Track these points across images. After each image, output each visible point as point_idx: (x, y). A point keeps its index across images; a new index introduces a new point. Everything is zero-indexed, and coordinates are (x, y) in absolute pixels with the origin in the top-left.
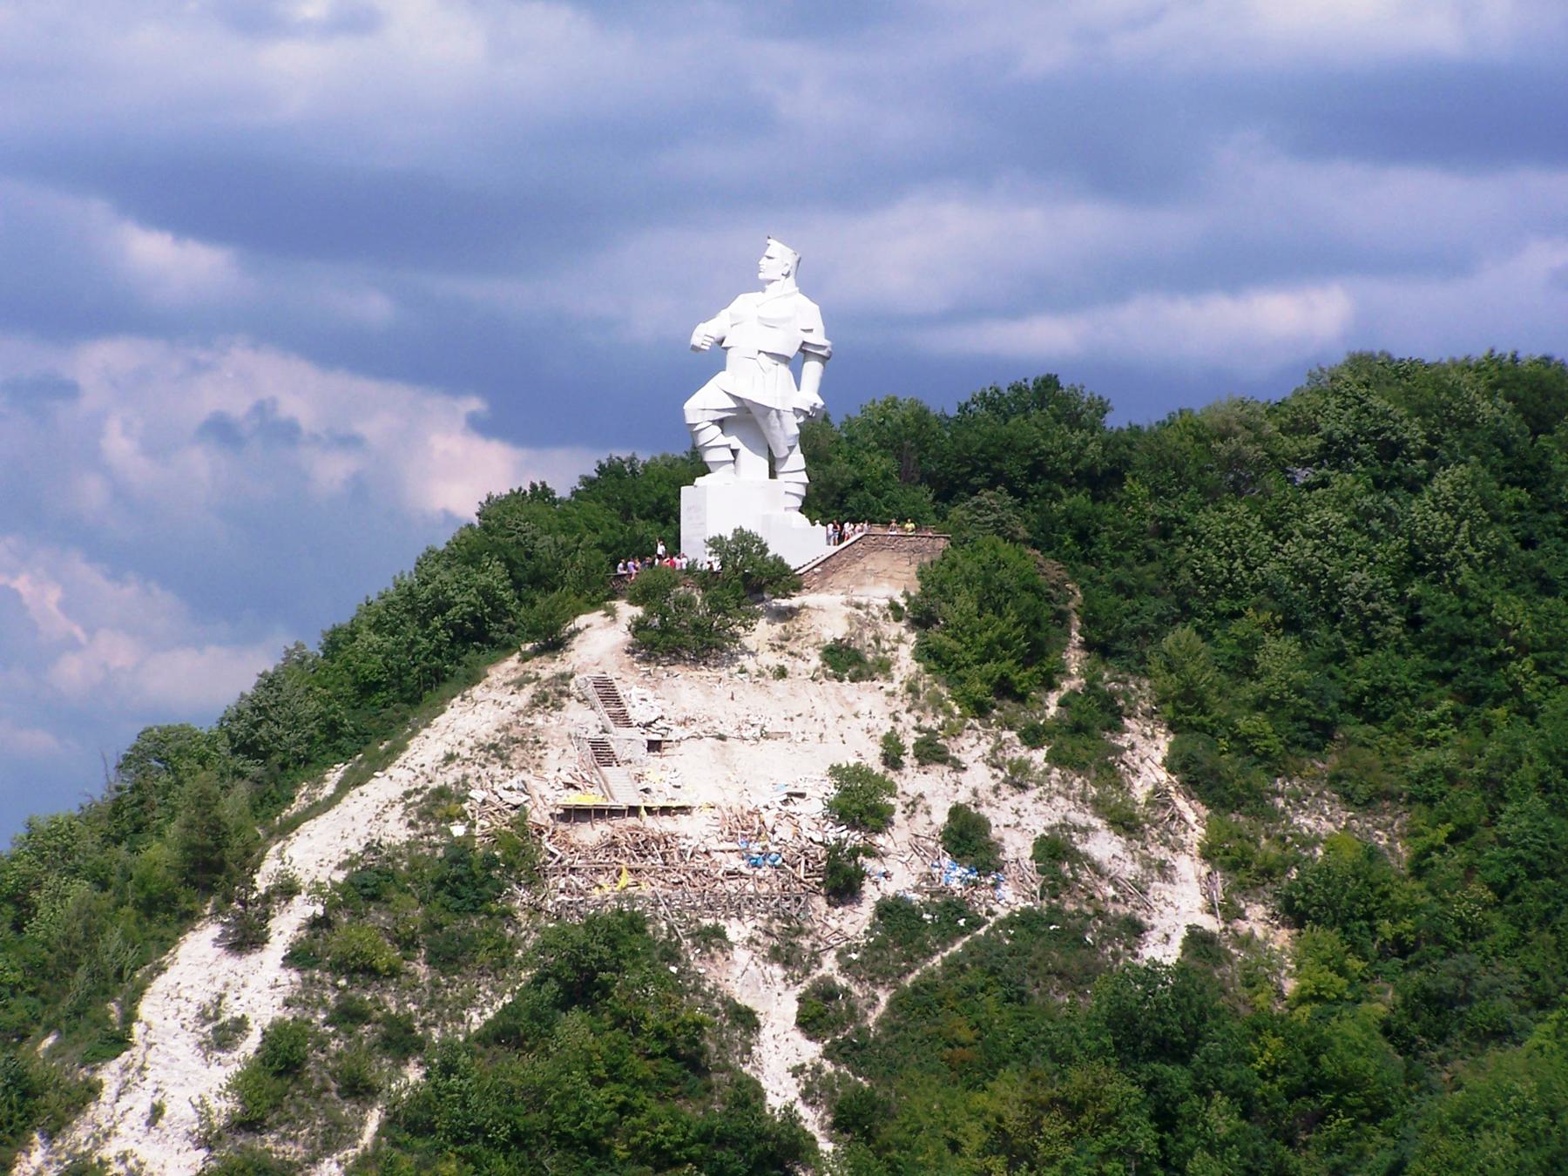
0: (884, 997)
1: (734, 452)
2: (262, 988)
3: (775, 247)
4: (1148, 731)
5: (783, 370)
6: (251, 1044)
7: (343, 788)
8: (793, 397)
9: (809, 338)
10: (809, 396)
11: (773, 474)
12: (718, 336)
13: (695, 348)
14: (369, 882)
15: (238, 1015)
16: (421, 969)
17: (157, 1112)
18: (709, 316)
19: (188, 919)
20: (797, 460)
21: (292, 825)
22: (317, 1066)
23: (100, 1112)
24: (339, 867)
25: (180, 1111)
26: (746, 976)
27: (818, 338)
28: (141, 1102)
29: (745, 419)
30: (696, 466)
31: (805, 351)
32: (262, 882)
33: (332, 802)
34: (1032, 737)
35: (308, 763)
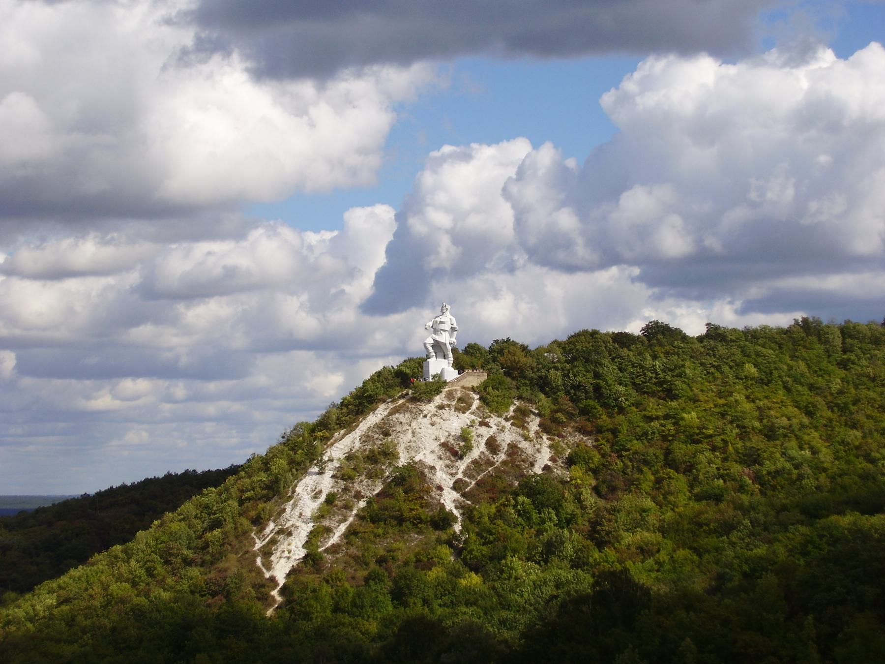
0: (473, 482)
2: (327, 483)
4: (380, 531)
6: (323, 498)
20: (451, 355)
21: (332, 444)
23: (286, 515)
26: (442, 477)
27: (455, 326)
28: (297, 512)
32: (325, 458)
34: (507, 419)
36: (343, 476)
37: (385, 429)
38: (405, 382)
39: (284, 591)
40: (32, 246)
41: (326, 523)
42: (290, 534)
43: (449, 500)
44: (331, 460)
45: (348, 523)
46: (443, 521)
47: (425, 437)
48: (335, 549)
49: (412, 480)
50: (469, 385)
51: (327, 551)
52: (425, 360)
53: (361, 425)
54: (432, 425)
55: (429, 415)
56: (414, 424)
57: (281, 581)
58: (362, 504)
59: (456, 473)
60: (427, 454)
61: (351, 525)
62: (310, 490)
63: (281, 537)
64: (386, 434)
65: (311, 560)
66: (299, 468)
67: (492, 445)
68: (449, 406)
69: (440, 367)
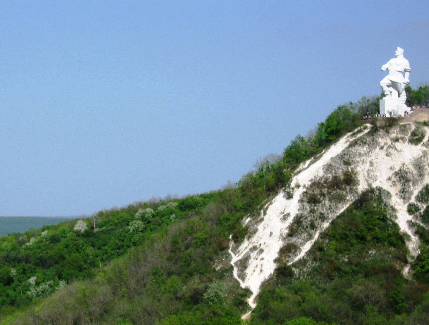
1: (391, 92)
2: (293, 207)
3: (399, 48)
5: (401, 74)
6: (290, 220)
7: (309, 165)
8: (403, 80)
9: (406, 68)
10: (407, 80)
11: (399, 96)
12: (387, 68)
13: (382, 71)
14: (315, 184)
15: (288, 212)
16: (327, 202)
17: (271, 234)
18: (385, 62)
19: (277, 193)
22: (306, 223)
24: (309, 181)
25: (277, 233)
27: (408, 67)
28: (268, 232)
29: (394, 85)
30: (383, 95)
31: (405, 71)
32: (293, 184)
33: (308, 167)
36: (311, 199)
37: (345, 159)
39: (255, 300)
40: (81, 278)
41: (294, 240)
44: (298, 186)
45: (313, 241)
48: (302, 262)
49: (371, 204)
50: (422, 120)
51: (294, 265)
52: (378, 100)
53: (324, 155)
54: (387, 155)
55: (385, 148)
56: (373, 155)
57: (255, 290)
58: (326, 225)
59: (410, 198)
60: (383, 180)
61: (316, 243)
62: (279, 213)
63: (253, 255)
64: (347, 163)
65: (283, 272)
66: (272, 191)
68: (402, 138)
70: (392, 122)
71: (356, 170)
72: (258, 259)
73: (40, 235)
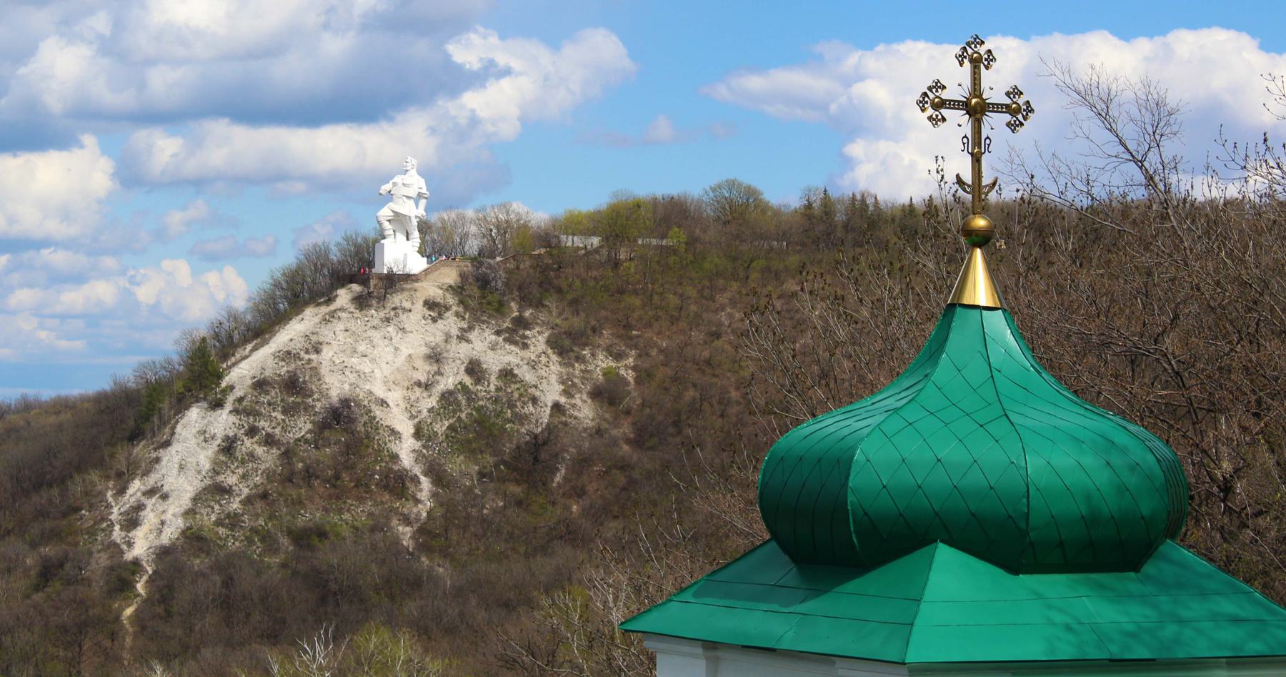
2: (223, 422)
5: (412, 202)
8: (414, 211)
10: (421, 212)
14: (261, 385)
20: (416, 234)
27: (424, 191)
29: (398, 219)
31: (420, 195)
35: (246, 341)
38: (350, 274)
42: (165, 497)
43: (406, 451)
46: (399, 484)
47: (386, 367)
49: (345, 420)
52: (376, 241)
63: (150, 503)
67: (474, 369)
69: (400, 254)
70: (394, 281)
71: (249, 317)
72: (169, 495)
73: (356, 341)
